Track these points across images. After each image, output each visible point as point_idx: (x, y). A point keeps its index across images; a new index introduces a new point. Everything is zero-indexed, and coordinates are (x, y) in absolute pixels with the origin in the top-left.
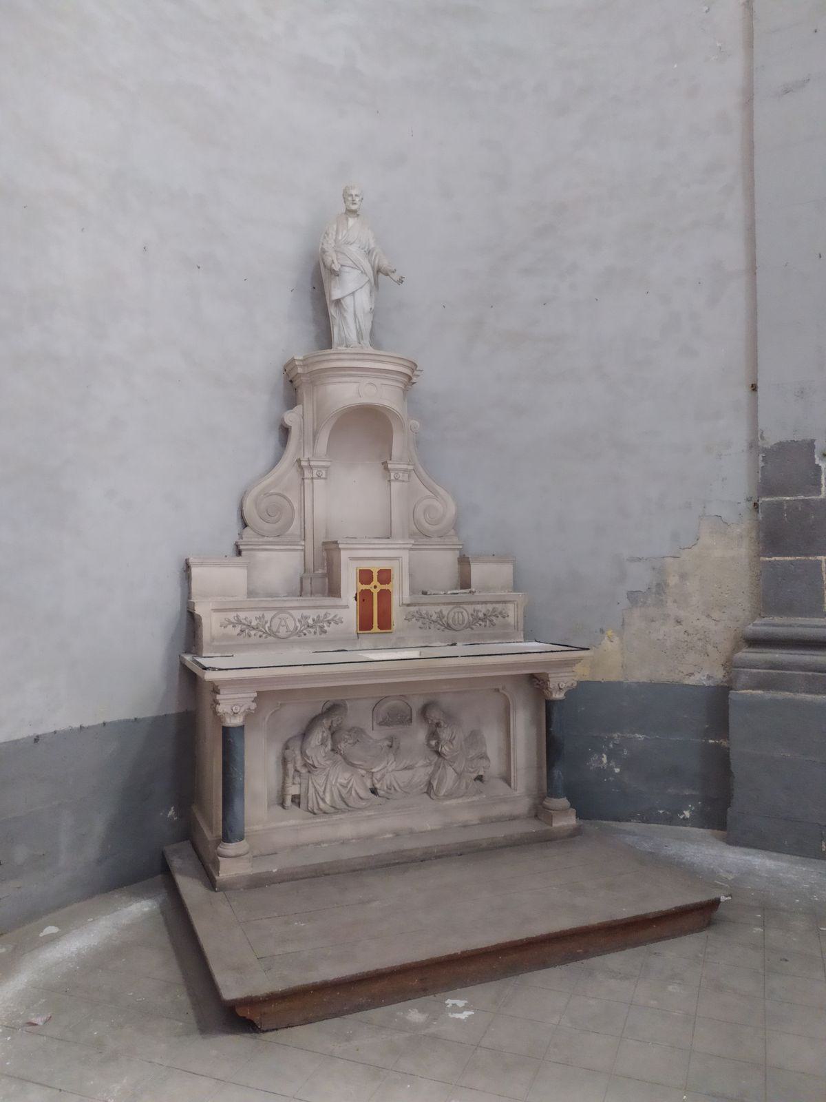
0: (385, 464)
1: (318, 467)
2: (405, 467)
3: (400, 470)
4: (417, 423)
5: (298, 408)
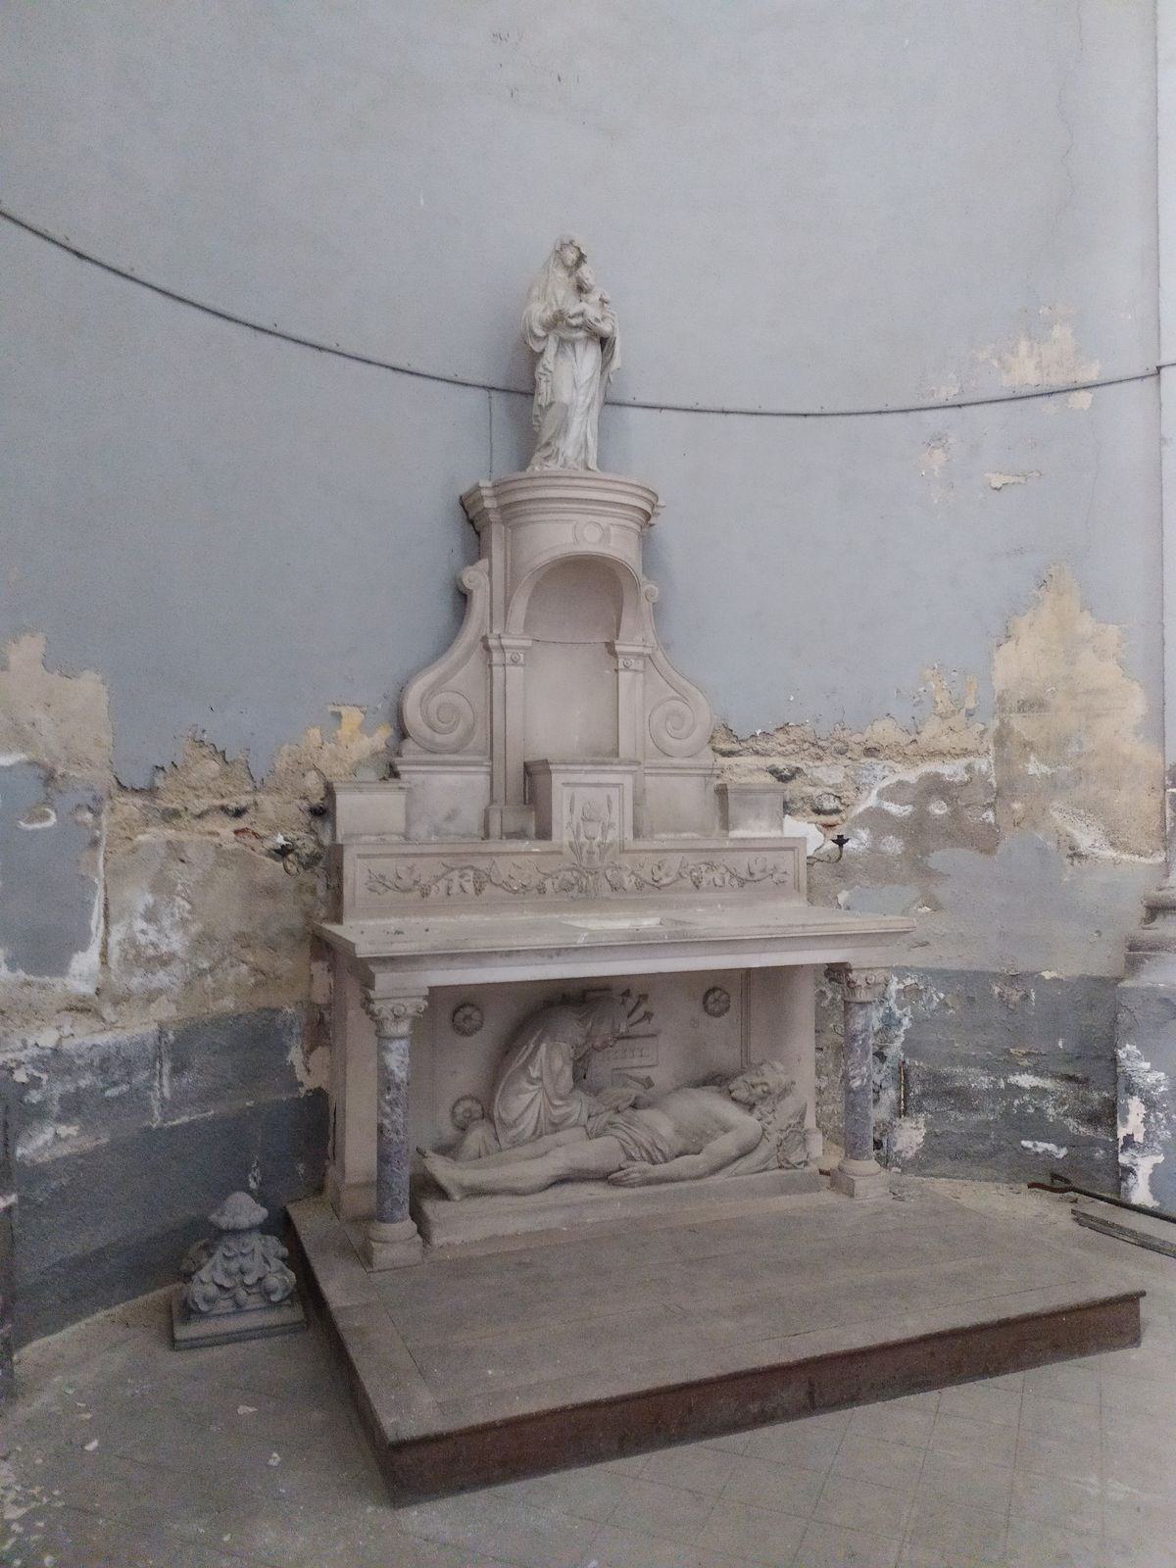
0: (610, 648)
1: (511, 647)
2: (639, 650)
3: (632, 654)
4: (657, 589)
5: (483, 563)
